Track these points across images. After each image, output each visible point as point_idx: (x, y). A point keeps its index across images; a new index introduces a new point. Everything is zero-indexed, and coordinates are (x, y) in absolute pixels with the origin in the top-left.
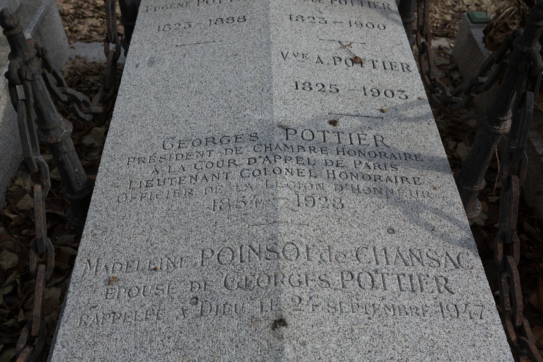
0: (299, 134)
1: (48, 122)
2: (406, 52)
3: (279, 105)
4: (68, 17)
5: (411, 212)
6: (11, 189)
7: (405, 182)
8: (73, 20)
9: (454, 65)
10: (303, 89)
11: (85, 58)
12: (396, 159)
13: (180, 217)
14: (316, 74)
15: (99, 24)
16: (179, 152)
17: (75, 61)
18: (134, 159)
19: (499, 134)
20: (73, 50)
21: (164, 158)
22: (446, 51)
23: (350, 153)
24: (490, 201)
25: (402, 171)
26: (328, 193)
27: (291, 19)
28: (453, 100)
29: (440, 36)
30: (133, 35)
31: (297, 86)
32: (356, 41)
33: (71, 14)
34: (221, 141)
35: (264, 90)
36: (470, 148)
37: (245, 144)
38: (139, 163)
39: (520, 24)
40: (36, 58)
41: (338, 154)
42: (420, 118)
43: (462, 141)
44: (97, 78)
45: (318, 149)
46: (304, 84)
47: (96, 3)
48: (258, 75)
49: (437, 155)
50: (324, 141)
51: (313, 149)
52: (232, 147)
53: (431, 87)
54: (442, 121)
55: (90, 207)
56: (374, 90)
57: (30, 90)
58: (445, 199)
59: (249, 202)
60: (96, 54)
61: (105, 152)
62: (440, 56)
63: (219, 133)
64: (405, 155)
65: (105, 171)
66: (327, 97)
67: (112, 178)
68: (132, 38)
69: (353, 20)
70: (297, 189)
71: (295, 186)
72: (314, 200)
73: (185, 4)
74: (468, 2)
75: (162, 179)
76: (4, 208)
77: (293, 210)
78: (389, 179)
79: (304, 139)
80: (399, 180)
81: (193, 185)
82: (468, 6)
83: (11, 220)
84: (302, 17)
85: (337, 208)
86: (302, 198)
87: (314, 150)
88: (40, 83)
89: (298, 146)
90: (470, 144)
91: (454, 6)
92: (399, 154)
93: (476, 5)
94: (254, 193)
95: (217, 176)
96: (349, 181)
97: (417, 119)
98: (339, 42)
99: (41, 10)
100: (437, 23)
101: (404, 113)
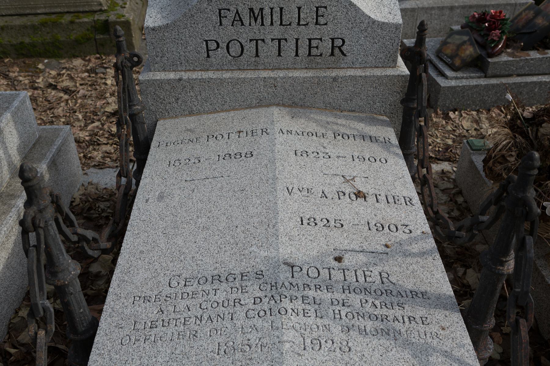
0: (305, 271)
1: (57, 264)
2: (408, 186)
3: (284, 241)
4: (84, 144)
5: (420, 355)
6: (14, 321)
7: (413, 322)
8: (88, 147)
9: (457, 189)
10: (308, 224)
11: (97, 184)
12: (402, 297)
13: (184, 362)
14: (321, 209)
15: (113, 151)
16: (185, 291)
17: (87, 187)
18: (140, 297)
19: (503, 275)
20: (86, 176)
21: (170, 297)
22: (449, 175)
23: (356, 291)
24: (504, 332)
25: (409, 310)
26: (334, 335)
27: (296, 154)
28: (456, 235)
29: (442, 160)
30: (144, 170)
31: (302, 221)
32: (359, 175)
33: (87, 141)
34: (227, 279)
35: (270, 226)
36: (479, 275)
37: (251, 282)
38: (144, 301)
39: (518, 156)
40: (51, 204)
41: (344, 292)
42: (425, 253)
43: (471, 267)
44: (108, 204)
45: (324, 287)
46: (309, 220)
47: (111, 131)
48: (264, 211)
49: (444, 292)
50: (330, 279)
51: (319, 287)
52: (238, 285)
53: (434, 219)
54: (449, 246)
55: (93, 349)
56: (378, 225)
57: (42, 237)
58: (455, 340)
59: (254, 345)
60: (108, 181)
61: (110, 290)
62: (444, 180)
63: (225, 271)
64: (411, 292)
65: (110, 310)
66: (332, 233)
67: (117, 319)
68: (144, 173)
69: (356, 154)
70: (303, 331)
71: (300, 328)
72: (320, 343)
73: (195, 140)
74: (468, 127)
75: (166, 320)
76: (5, 342)
77: (299, 355)
78: (396, 319)
79: (309, 277)
80: (406, 320)
81: (197, 327)
82: (467, 131)
83: (11, 355)
84: (307, 152)
85: (344, 352)
86: (308, 341)
87: (319, 289)
88: (52, 228)
89: (304, 285)
90: (479, 270)
91: (454, 130)
92: (406, 292)
93: (475, 129)
94: (259, 335)
95: (222, 317)
96: (356, 322)
97: (423, 254)
98: (342, 176)
99: (58, 142)
100: (439, 147)
101: (409, 248)
